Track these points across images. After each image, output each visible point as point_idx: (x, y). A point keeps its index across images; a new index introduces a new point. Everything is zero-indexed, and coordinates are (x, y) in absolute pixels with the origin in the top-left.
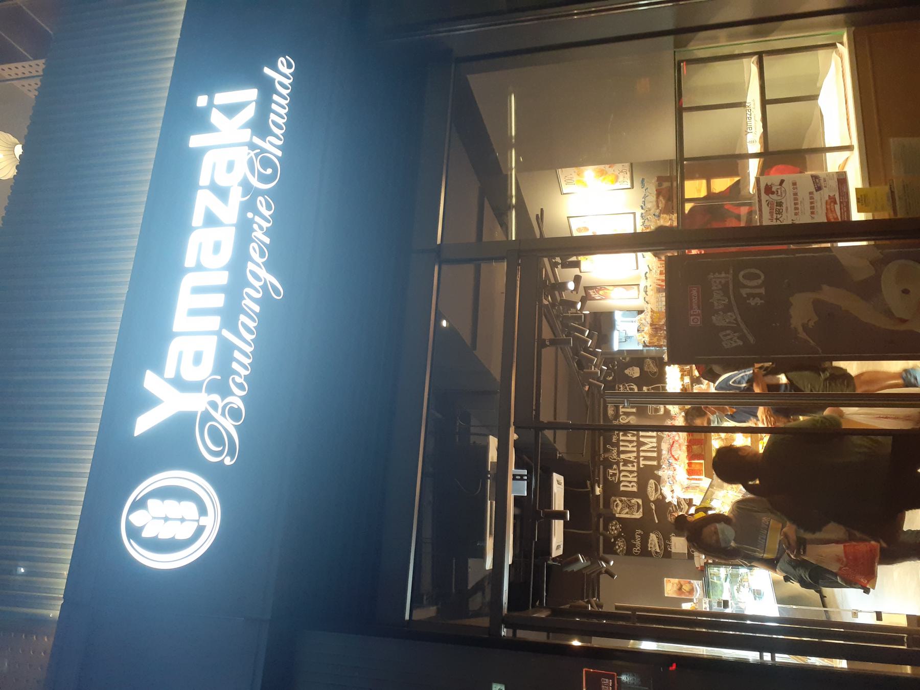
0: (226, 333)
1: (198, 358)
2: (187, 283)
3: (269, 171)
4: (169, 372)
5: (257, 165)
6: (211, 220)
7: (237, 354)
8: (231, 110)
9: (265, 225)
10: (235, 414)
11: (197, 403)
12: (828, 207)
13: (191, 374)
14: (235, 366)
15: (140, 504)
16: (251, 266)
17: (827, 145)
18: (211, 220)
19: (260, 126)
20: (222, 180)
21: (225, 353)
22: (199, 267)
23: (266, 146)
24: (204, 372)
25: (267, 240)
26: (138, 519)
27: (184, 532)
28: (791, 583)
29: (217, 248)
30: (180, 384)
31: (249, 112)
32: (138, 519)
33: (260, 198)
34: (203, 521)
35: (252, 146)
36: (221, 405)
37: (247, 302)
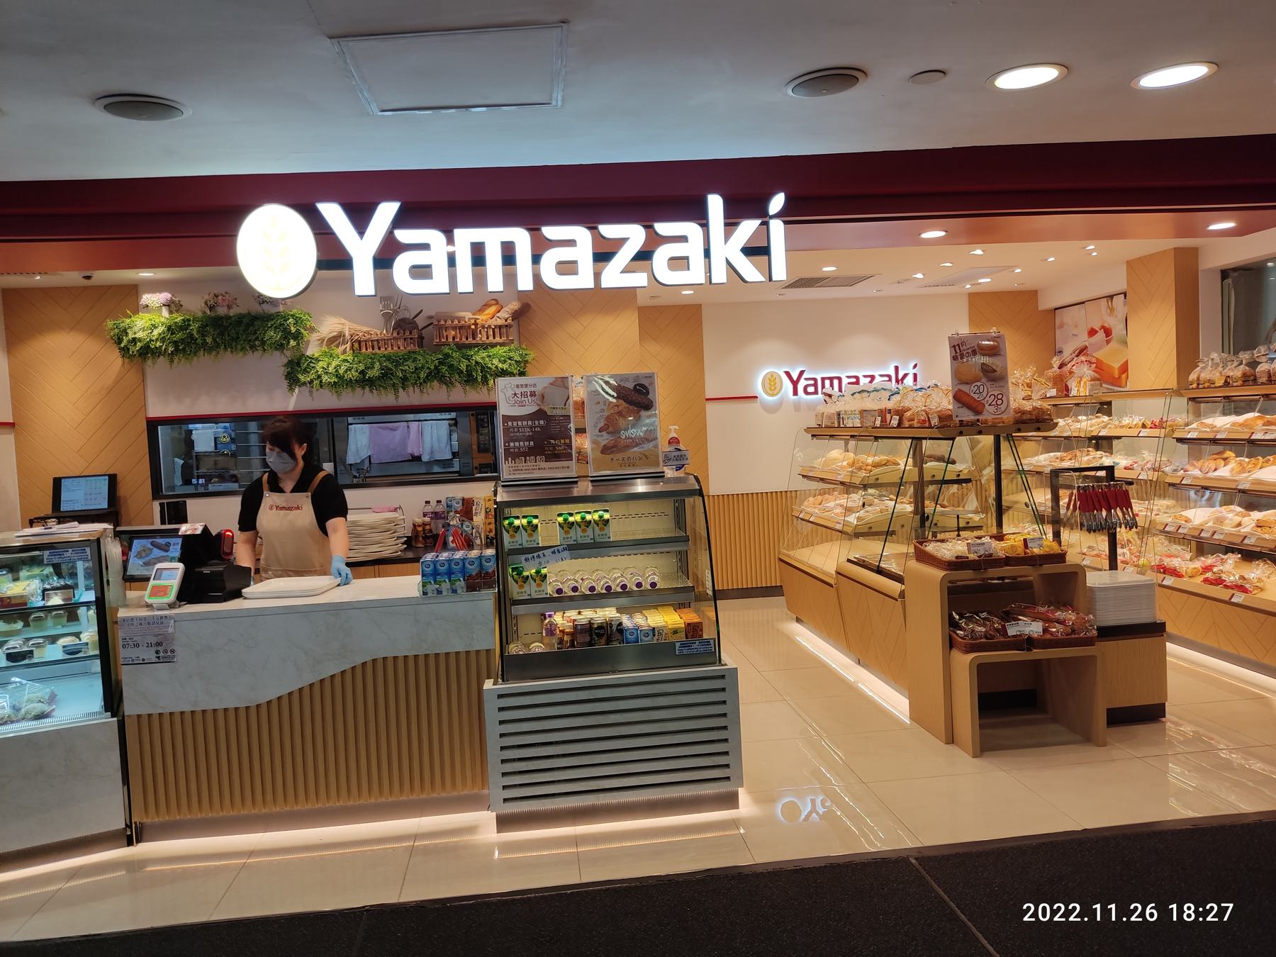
2: (520, 237)
4: (403, 236)
6: (603, 255)
13: (403, 263)
18: (603, 255)
20: (662, 255)
22: (540, 247)
29: (567, 268)
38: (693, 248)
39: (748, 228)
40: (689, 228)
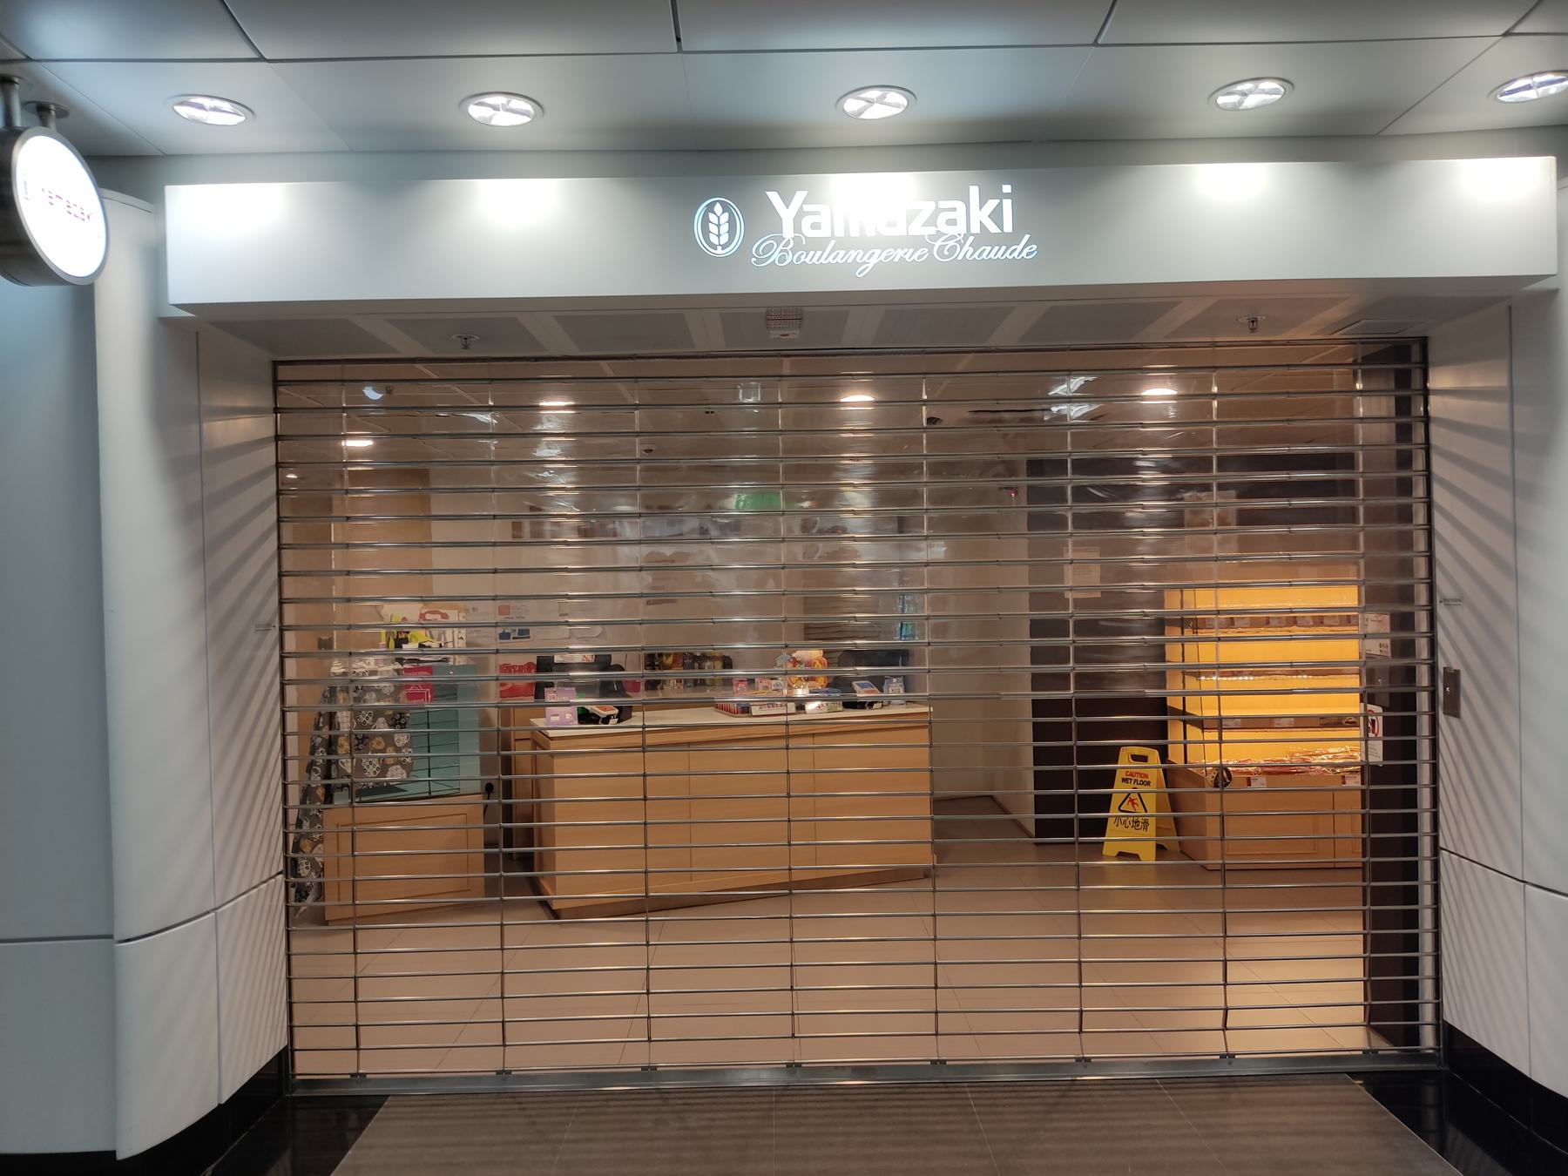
0: (833, 242)
1: (815, 226)
3: (946, 253)
4: (806, 208)
5: (951, 243)
7: (819, 253)
8: (996, 215)
9: (907, 257)
10: (782, 259)
11: (788, 232)
12: (1070, 640)
13: (806, 223)
14: (812, 253)
15: (726, 208)
16: (878, 252)
17: (435, 567)
19: (984, 238)
21: (819, 244)
23: (966, 247)
24: (808, 231)
25: (896, 260)
26: (718, 208)
27: (714, 239)
28: (286, 496)
30: (800, 215)
31: (993, 229)
32: (718, 208)
33: (927, 250)
34: (720, 248)
35: (966, 237)
36: (787, 248)
37: (853, 253)
38: (960, 215)
39: (992, 204)
40: (960, 205)
